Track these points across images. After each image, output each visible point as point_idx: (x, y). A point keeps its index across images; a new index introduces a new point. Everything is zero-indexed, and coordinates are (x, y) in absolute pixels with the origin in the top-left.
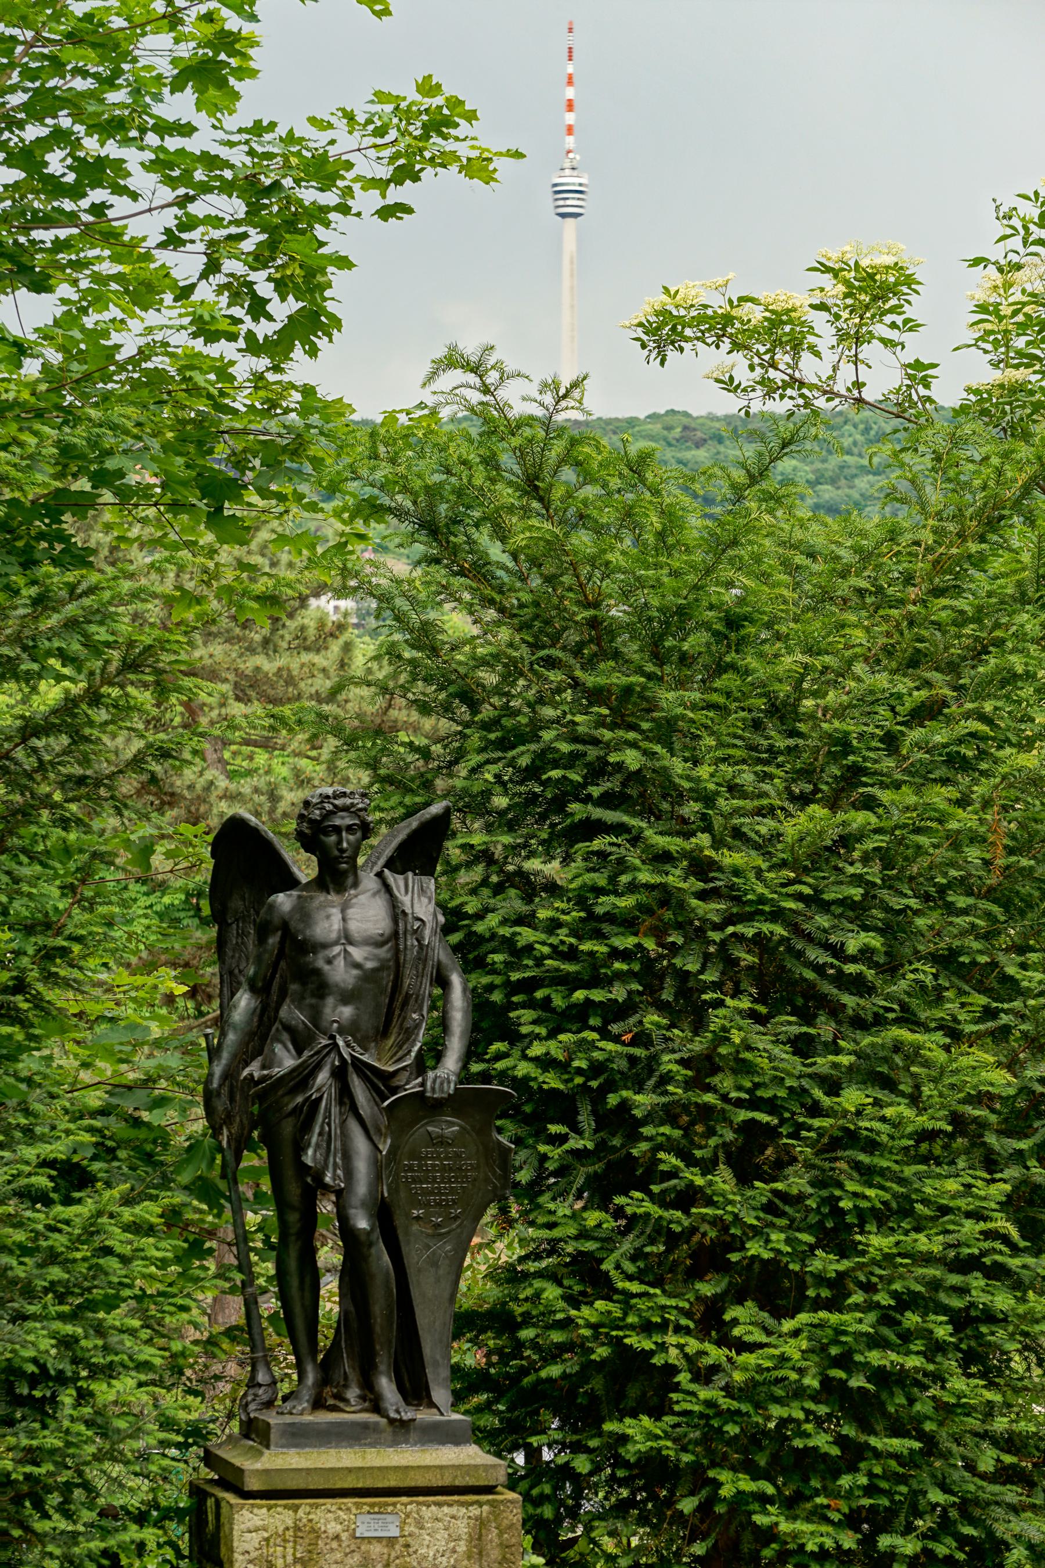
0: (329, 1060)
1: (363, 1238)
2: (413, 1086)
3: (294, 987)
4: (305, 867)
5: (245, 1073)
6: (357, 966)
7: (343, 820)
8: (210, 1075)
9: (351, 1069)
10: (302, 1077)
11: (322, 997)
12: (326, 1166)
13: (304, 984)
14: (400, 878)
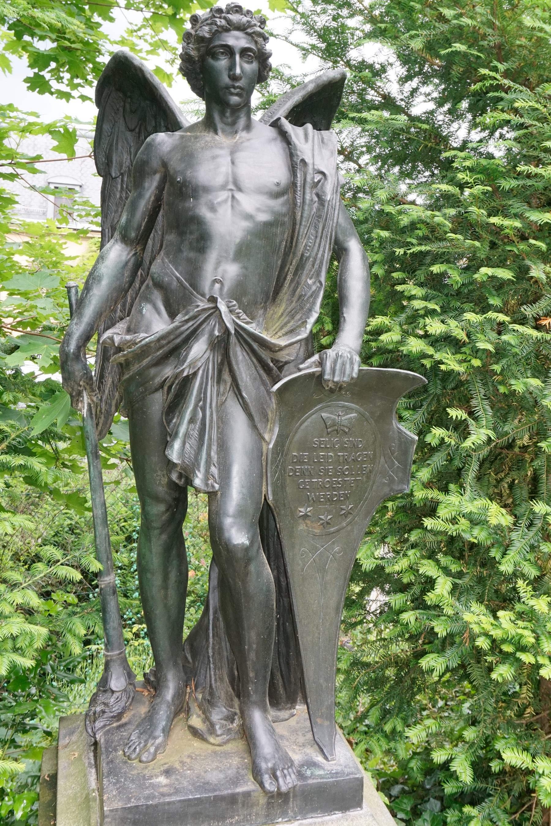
0: (206, 327)
1: (240, 555)
2: (309, 367)
3: (171, 237)
4: (183, 99)
6: (249, 217)
7: (236, 40)
9: (233, 339)
10: (174, 347)
12: (196, 464)
13: (182, 234)
14: (300, 130)
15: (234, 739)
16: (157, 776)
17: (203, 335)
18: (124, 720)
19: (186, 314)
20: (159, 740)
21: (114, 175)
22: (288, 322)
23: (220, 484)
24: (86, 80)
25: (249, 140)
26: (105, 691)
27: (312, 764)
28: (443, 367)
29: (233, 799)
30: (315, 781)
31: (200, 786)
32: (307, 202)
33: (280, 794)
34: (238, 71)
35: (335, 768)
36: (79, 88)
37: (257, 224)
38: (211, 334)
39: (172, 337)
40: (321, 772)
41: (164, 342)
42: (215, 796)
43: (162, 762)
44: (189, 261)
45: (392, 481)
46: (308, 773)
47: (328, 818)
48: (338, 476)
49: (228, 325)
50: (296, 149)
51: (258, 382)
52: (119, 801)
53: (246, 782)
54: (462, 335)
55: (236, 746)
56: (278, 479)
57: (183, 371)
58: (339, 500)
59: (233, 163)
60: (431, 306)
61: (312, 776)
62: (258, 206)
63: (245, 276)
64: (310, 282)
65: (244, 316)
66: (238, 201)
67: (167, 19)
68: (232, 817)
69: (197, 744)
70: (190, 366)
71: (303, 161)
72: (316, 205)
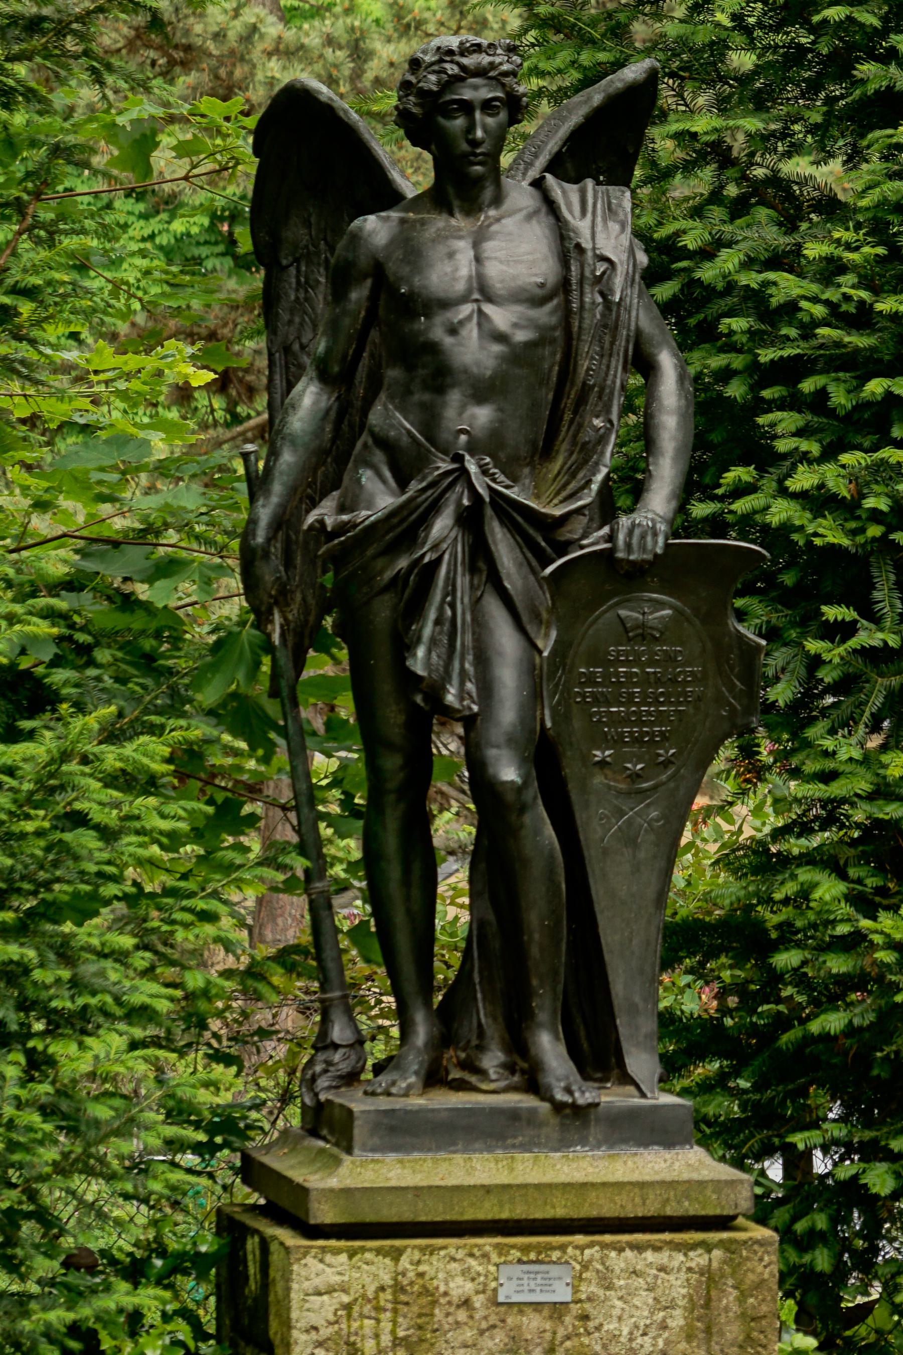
0: (452, 497)
1: (510, 797)
2: (594, 541)
3: (393, 374)
5: (311, 518)
6: (500, 337)
7: (475, 92)
8: (252, 522)
9: (489, 512)
10: (407, 526)
13: (410, 368)
17: (447, 506)
21: (284, 262)
22: (567, 483)
23: (479, 705)
28: (818, 541)
32: (587, 306)
38: (459, 503)
39: (405, 513)
41: (395, 521)
48: (649, 705)
49: (480, 490)
51: (526, 569)
54: (844, 491)
56: (559, 703)
58: (652, 741)
63: (501, 421)
65: (502, 478)
68: (515, 1137)
71: (578, 246)
72: (600, 308)
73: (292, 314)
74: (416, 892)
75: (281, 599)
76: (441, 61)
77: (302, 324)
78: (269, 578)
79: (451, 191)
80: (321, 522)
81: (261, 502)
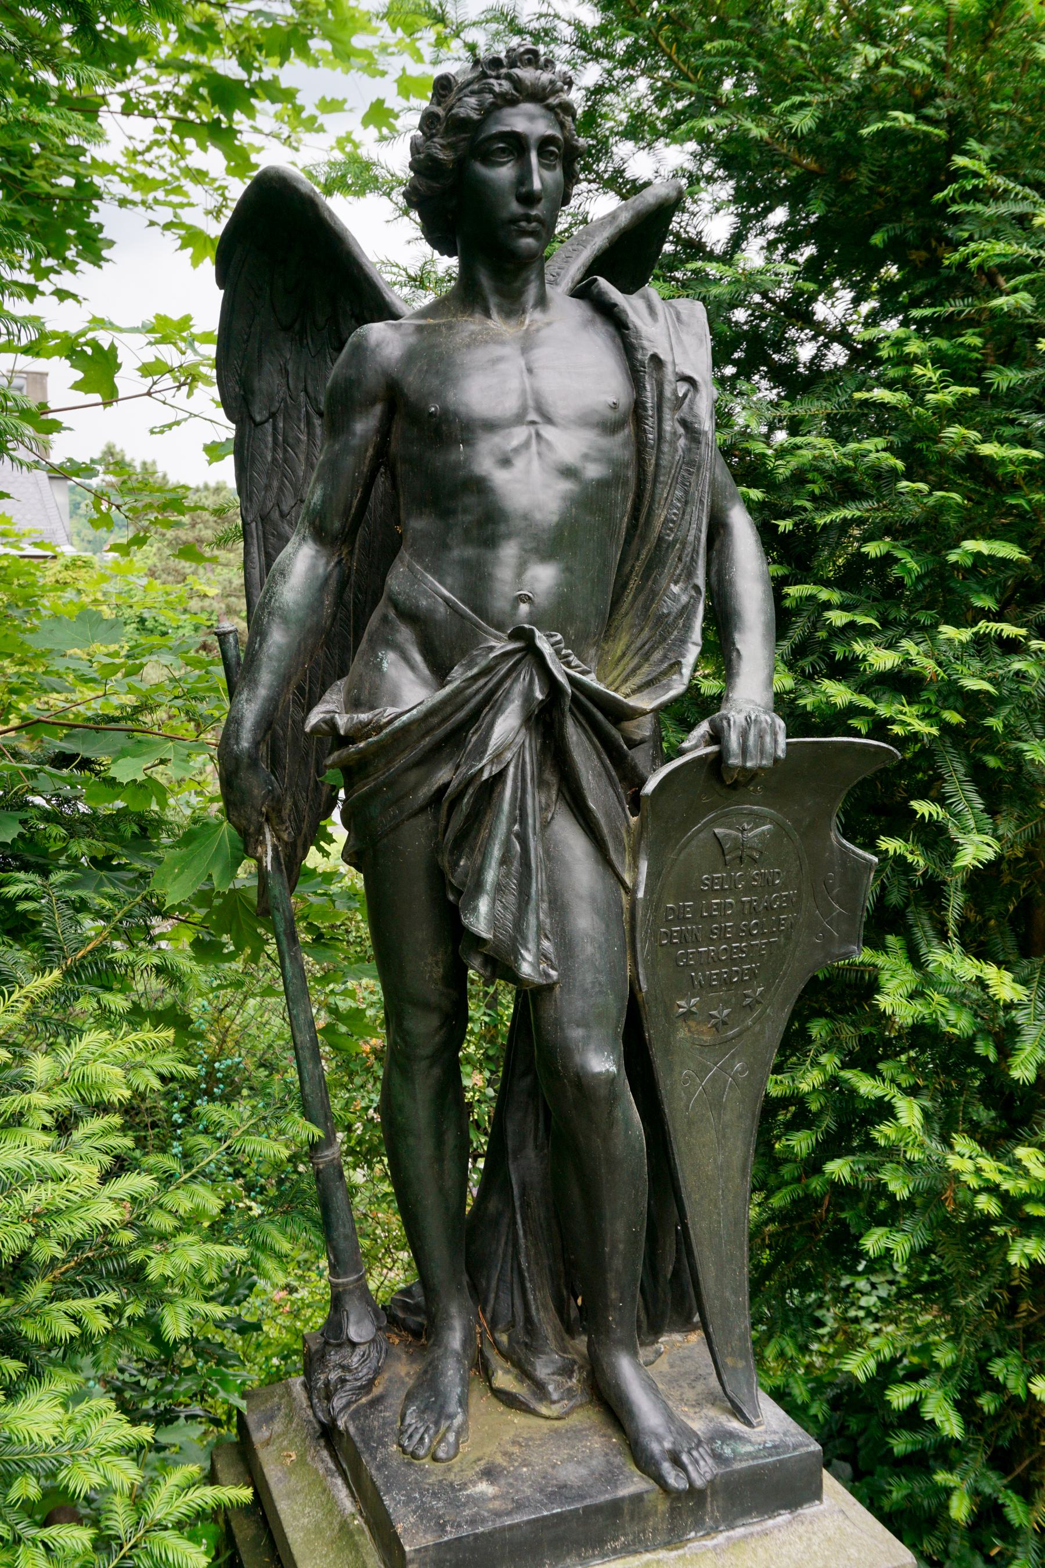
0: (519, 688)
5: (315, 717)
7: (527, 121)
8: (234, 722)
10: (454, 729)
11: (491, 542)
15: (581, 1406)
16: (474, 1484)
18: (377, 1391)
19: (469, 667)
20: (458, 1421)
21: (258, 418)
24: (65, 259)
25: (549, 324)
26: (340, 1346)
27: (730, 1436)
29: (615, 1508)
30: (744, 1464)
31: (553, 1493)
32: (668, 436)
33: (693, 1492)
34: (537, 185)
35: (767, 1438)
36: (52, 276)
37: (585, 485)
38: (528, 696)
39: (449, 709)
40: (749, 1448)
41: (435, 720)
42: (585, 1508)
43: (472, 1457)
44: (466, 565)
45: (828, 938)
46: (727, 1451)
47: (770, 1523)
50: (639, 337)
51: (605, 779)
52: (425, 1532)
53: (629, 1478)
55: (586, 1418)
57: (482, 770)
59: (530, 371)
60: (862, 620)
61: (737, 1456)
62: (585, 450)
63: (570, 585)
64: (675, 589)
66: (548, 443)
67: (204, 131)
69: (518, 1419)
70: (492, 762)
71: (656, 359)
72: (682, 442)
73: (269, 476)
74: (449, 1165)
75: (273, 816)
76: (484, 75)
77: (281, 489)
78: (258, 792)
79: (486, 282)
80: (332, 724)
81: (244, 696)
